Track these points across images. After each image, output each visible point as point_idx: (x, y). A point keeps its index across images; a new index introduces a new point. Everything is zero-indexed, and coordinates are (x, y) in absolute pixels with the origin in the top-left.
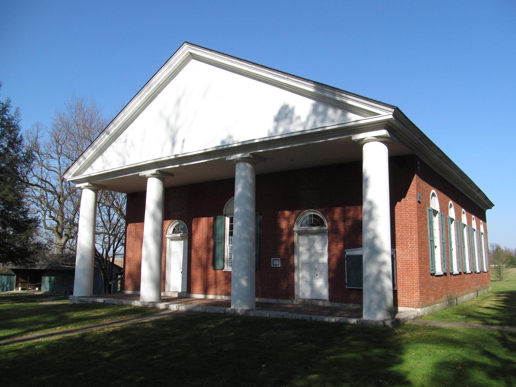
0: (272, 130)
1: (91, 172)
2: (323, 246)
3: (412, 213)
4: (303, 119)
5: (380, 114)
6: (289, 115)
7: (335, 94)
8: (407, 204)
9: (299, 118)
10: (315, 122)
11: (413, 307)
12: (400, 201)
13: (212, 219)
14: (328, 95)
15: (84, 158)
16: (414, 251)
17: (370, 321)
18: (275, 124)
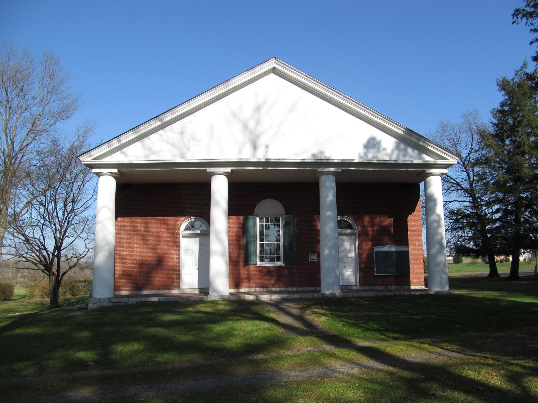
0: (362, 154)
1: (118, 158)
2: (351, 245)
3: (419, 223)
4: (389, 151)
5: (449, 160)
6: (377, 146)
7: (420, 140)
8: (415, 217)
9: (385, 149)
10: (398, 155)
11: (420, 285)
12: (411, 214)
13: (242, 218)
15: (119, 141)
16: (420, 248)
17: (441, 291)
18: (365, 150)
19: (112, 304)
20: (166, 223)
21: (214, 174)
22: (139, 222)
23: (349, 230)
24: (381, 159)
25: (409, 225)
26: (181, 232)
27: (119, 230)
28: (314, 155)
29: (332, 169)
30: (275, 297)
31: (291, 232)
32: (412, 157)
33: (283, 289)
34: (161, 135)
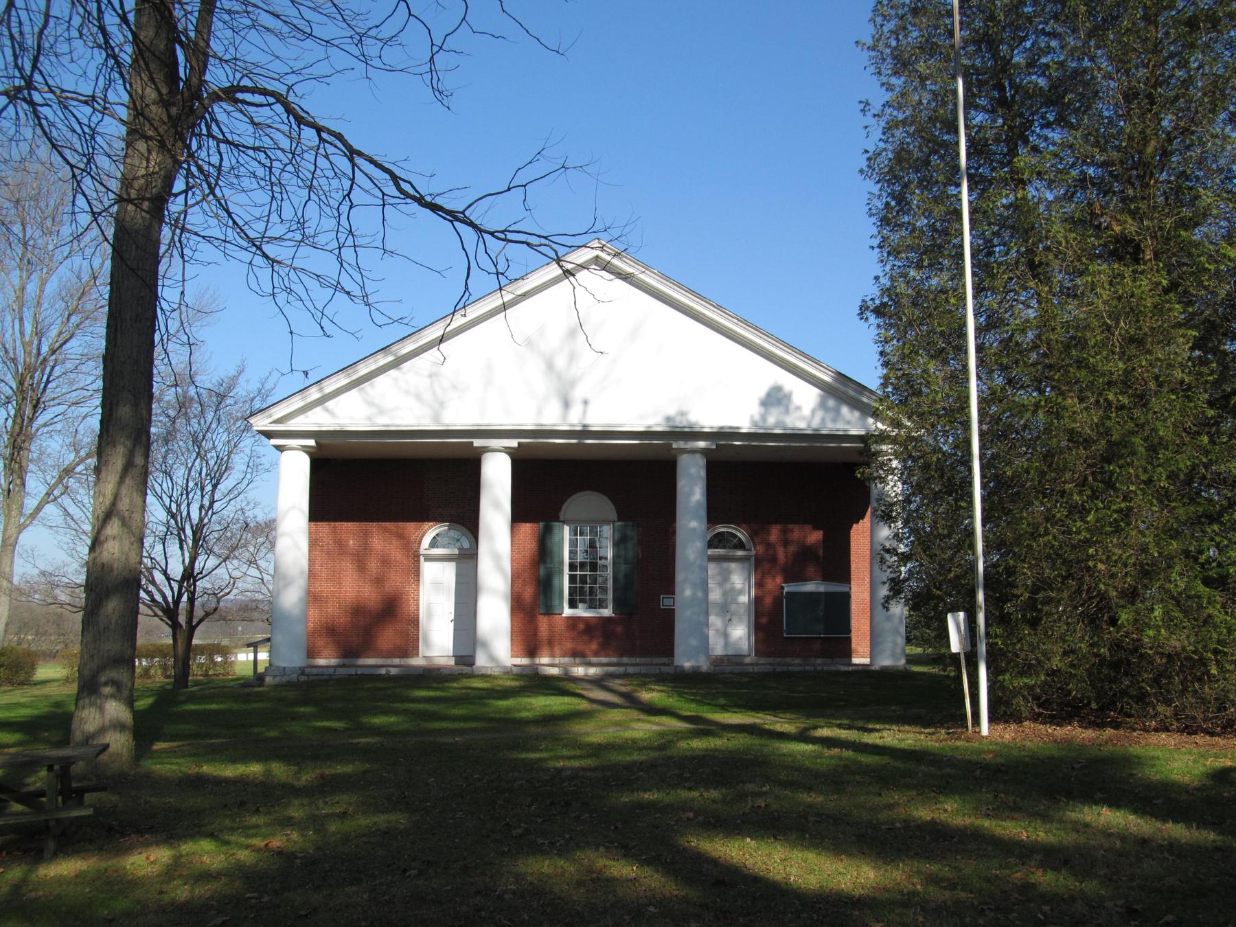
0: (757, 418)
4: (806, 411)
6: (785, 402)
7: (861, 393)
10: (823, 420)
14: (851, 392)
15: (321, 390)
18: (762, 410)
19: (306, 678)
20: (401, 536)
21: (486, 450)
22: (349, 531)
23: (740, 553)
24: (790, 426)
25: (853, 544)
26: (422, 551)
27: (313, 543)
28: (668, 419)
29: (702, 444)
30: (592, 671)
31: (631, 554)
32: (848, 423)
33: (614, 660)
34: (396, 380)
